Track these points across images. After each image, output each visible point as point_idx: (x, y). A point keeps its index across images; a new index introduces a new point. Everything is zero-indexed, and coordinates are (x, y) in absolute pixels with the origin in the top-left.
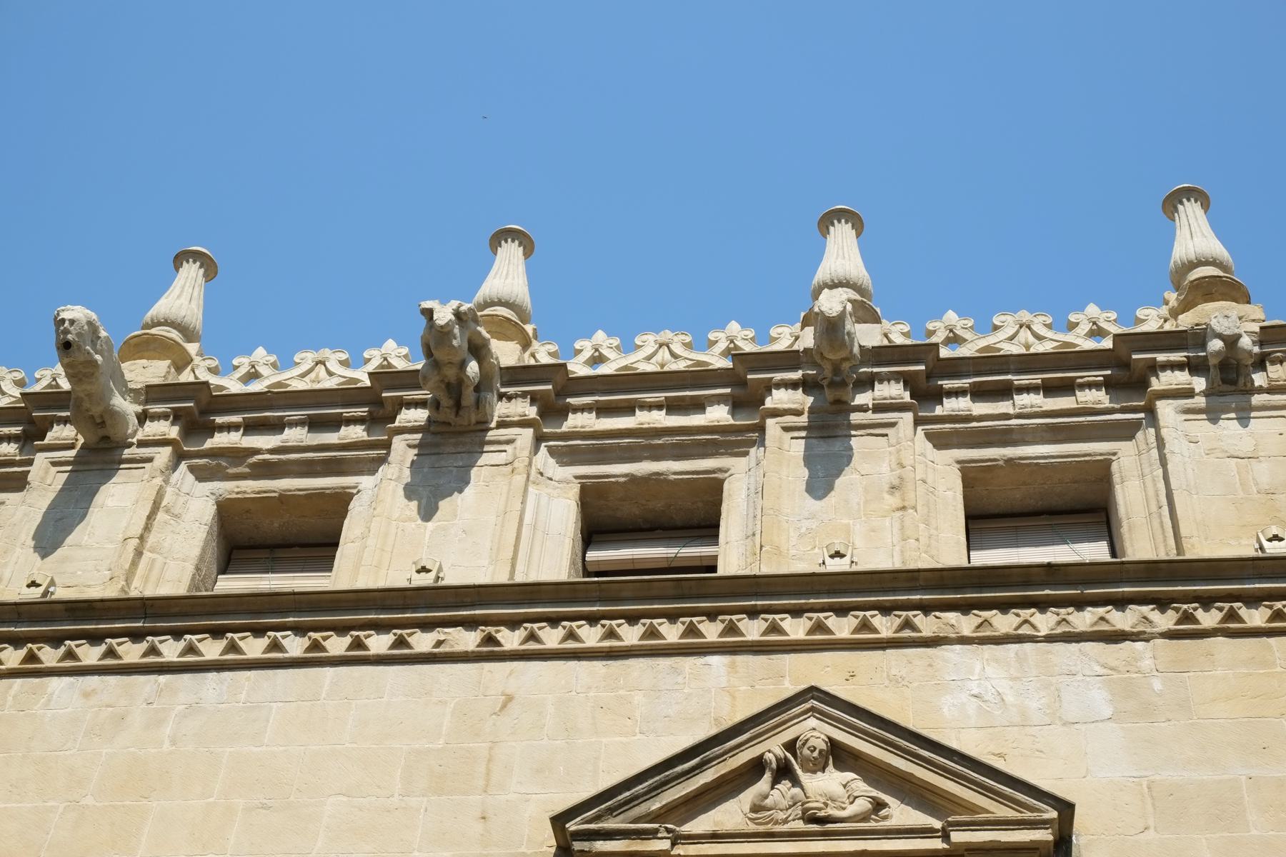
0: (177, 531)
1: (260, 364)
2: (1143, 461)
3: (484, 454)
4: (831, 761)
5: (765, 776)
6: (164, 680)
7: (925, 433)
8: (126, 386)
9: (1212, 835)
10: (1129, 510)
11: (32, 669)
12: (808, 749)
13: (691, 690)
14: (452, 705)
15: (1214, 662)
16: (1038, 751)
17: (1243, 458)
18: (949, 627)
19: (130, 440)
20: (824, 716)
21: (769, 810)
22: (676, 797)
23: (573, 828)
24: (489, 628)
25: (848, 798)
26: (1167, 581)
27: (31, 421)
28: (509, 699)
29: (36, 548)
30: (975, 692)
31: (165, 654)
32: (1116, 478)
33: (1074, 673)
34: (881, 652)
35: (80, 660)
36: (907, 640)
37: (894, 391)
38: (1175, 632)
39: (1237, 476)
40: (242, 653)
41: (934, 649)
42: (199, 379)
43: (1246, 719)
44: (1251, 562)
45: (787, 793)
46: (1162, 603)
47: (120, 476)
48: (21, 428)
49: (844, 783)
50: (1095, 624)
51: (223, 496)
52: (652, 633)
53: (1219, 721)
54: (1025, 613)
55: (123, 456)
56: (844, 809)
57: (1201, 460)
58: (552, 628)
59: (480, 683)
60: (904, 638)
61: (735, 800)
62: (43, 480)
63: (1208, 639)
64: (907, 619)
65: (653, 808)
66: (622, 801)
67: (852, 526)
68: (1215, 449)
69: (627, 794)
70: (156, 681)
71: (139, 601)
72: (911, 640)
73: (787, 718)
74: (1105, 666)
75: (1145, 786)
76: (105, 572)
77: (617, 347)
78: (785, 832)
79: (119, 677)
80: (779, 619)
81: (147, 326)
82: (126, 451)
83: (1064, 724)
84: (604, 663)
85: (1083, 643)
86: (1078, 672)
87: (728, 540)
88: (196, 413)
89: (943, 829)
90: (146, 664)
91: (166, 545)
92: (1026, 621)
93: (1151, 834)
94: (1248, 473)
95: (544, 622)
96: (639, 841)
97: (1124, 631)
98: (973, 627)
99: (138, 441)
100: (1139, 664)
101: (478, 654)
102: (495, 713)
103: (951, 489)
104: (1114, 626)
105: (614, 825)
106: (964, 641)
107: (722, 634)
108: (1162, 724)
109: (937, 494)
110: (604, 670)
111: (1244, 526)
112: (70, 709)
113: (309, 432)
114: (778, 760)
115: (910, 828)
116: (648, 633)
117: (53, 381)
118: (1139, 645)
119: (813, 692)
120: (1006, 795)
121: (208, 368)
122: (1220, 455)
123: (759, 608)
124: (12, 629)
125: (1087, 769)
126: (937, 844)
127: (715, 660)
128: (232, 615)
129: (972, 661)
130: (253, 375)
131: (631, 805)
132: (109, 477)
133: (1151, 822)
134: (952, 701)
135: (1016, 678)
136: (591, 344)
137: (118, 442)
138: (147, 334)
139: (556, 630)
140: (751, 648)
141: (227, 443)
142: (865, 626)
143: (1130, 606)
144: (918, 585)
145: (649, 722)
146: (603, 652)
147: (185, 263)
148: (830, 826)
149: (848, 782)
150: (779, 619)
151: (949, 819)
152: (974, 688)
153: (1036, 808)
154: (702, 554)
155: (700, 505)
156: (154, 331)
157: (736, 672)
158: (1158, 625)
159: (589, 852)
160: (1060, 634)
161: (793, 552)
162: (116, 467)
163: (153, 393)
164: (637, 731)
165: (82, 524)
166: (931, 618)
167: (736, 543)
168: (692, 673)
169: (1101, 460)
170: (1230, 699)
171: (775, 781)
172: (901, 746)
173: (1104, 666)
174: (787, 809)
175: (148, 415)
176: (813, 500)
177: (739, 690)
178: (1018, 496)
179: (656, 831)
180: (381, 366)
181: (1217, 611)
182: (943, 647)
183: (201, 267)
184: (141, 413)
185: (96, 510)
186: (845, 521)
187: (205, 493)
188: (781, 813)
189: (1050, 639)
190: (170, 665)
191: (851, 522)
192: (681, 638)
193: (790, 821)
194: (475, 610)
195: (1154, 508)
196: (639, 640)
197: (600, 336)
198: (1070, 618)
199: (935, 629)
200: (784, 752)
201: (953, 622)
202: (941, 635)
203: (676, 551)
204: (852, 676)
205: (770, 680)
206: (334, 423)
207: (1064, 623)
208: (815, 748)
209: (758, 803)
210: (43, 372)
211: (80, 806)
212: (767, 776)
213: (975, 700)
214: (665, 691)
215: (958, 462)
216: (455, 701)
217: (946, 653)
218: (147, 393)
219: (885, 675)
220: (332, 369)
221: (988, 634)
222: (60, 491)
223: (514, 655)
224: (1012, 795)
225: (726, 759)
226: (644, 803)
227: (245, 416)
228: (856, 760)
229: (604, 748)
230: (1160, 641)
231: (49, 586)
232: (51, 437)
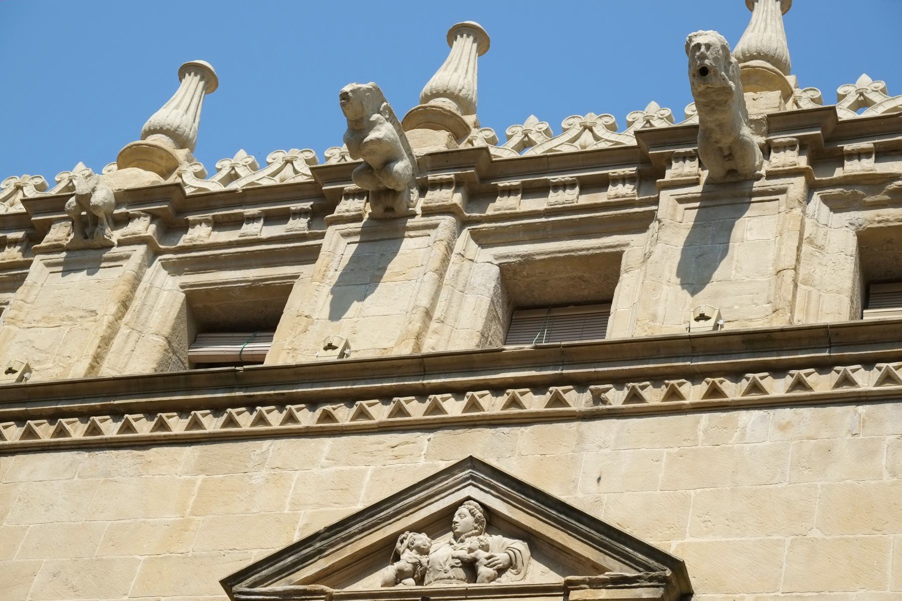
0: (824, 263)
3: (752, 205)
6: (864, 411)
7: (821, 197)
8: (747, 118)
11: (718, 402)
19: (758, 172)
27: (321, 195)
29: (684, 285)
31: (860, 384)
35: (766, 393)
37: (142, 227)
40: (522, 407)
42: (801, 107)
47: (754, 209)
48: (635, 168)
51: (863, 226)
55: (754, 189)
62: (673, 218)
70: (856, 412)
71: (824, 329)
76: (764, 305)
77: (883, 91)
79: (813, 408)
81: (427, 98)
82: (756, 184)
88: (477, 179)
90: (841, 394)
91: (817, 277)
99: (767, 172)
112: (768, 443)
113: (264, 224)
117: (232, 170)
121: (306, 160)
124: (688, 363)
128: (266, 387)
130: (233, 176)
132: (741, 212)
137: (746, 175)
138: (748, 66)
139: (783, 379)
141: (861, 170)
154: (254, 353)
156: (432, 103)
162: (748, 200)
163: (437, 160)
165: (726, 259)
175: (772, 146)
183: (201, 80)
184: (764, 145)
185: (737, 244)
187: (843, 224)
190: (868, 395)
192: (664, 400)
197: (864, 81)
206: (602, 184)
210: (635, 115)
211: (808, 539)
215: (182, 287)
218: (769, 123)
220: (297, 168)
222: (692, 228)
227: (876, 141)
231: (344, 349)
232: (670, 175)
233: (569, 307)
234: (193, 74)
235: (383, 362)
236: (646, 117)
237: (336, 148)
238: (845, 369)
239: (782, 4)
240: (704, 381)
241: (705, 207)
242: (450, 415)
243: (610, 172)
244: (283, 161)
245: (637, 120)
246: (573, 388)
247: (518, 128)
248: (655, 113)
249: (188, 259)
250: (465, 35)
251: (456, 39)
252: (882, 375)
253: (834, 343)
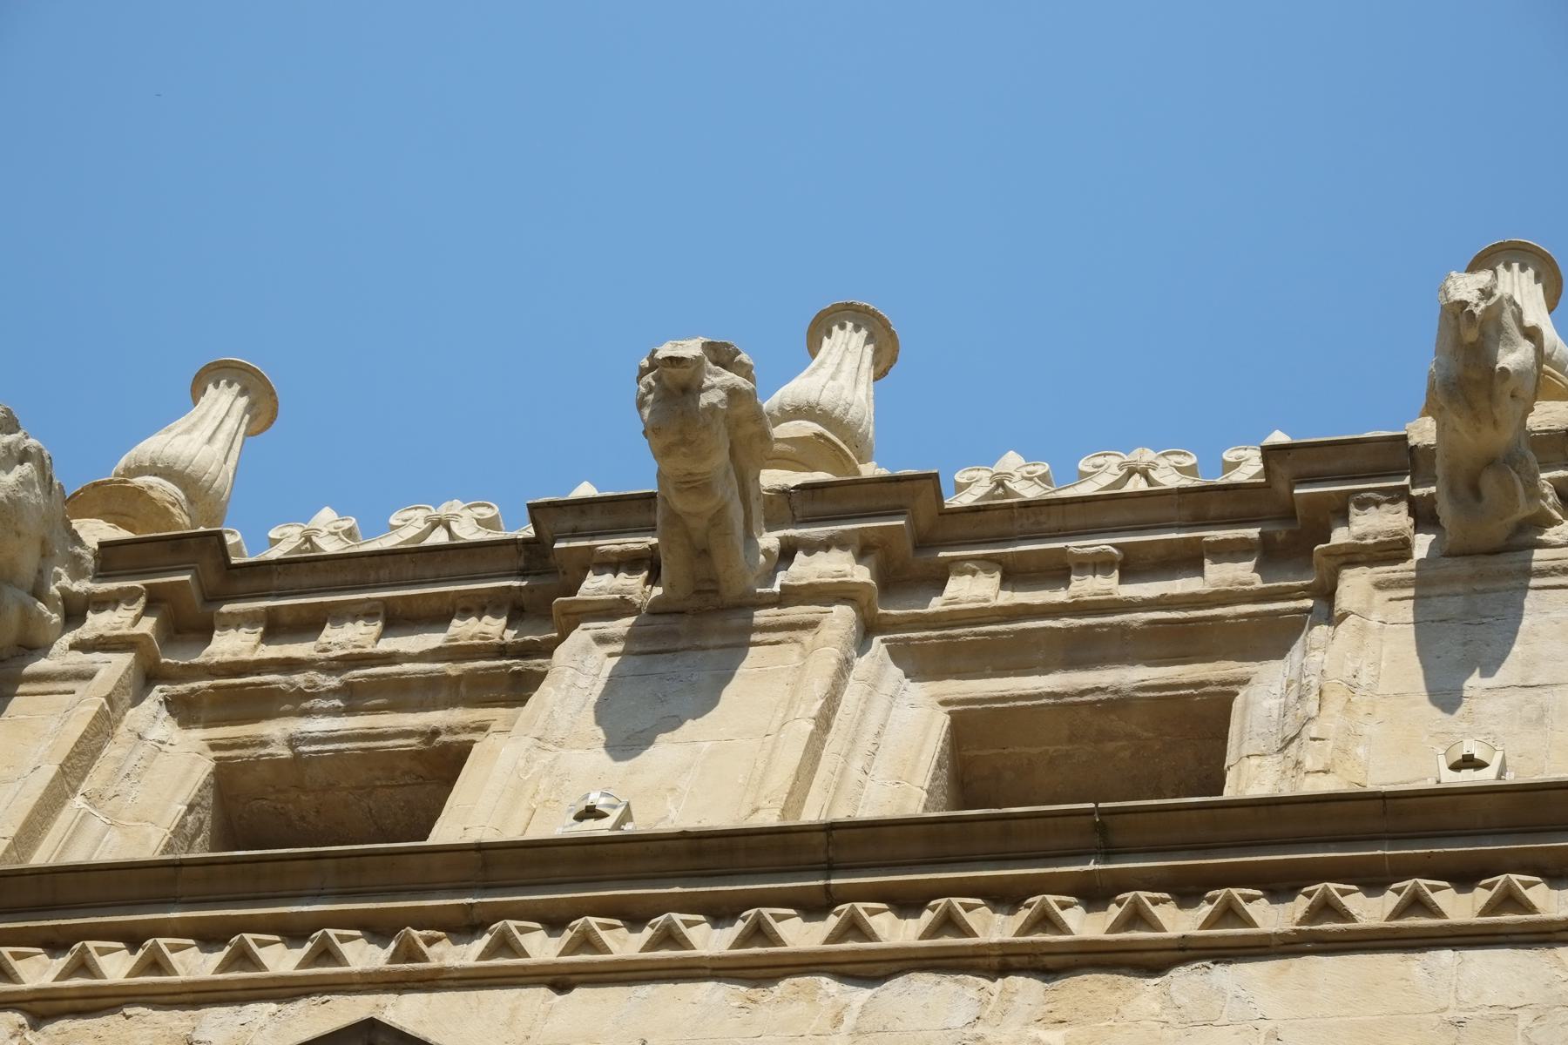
1: (321, 535)
27: (1288, 513)
35: (1162, 929)
64: (1325, 894)
95: (357, 929)
136: (990, 475)
139: (1470, 894)
140: (176, 998)
147: (210, 387)
156: (140, 481)
180: (298, 549)
183: (242, 393)
234: (850, 325)
235: (1350, 803)
236: (994, 476)
237: (979, 470)
239: (876, 352)
241: (1422, 597)
242: (790, 948)
243: (1074, 545)
244: (425, 523)
245: (977, 481)
246: (887, 907)
247: (981, 473)
248: (325, 526)
249: (917, 642)
250: (1516, 266)
251: (829, 334)
252: (746, 927)
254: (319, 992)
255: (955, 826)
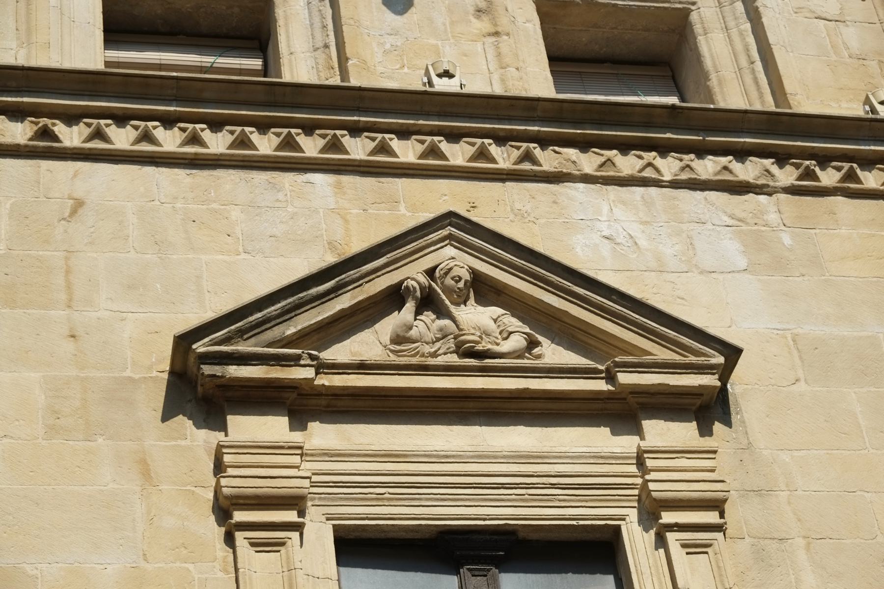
2: (725, 14)
4: (472, 294)
5: (407, 305)
9: (860, 390)
10: (717, 63)
11: (440, 166)
12: (452, 279)
13: (296, 210)
14: (8, 206)
15: (837, 221)
16: (679, 298)
17: (831, 21)
18: (570, 163)
20: (462, 245)
21: (414, 343)
22: (312, 322)
23: (202, 350)
24: (45, 119)
25: (501, 333)
26: (786, 135)
28: (79, 204)
30: (606, 233)
32: (698, 28)
33: (703, 221)
34: (500, 184)
36: (530, 174)
38: (798, 188)
39: (827, 37)
41: (556, 185)
43: (875, 279)
44: (868, 123)
45: (432, 325)
46: (782, 158)
49: (495, 317)
50: (719, 173)
52: (243, 142)
53: (850, 279)
54: (650, 156)
56: (498, 344)
57: (791, 18)
58: (119, 127)
59: (39, 183)
60: (525, 171)
61: (370, 330)
63: (828, 198)
64: (528, 151)
65: (289, 332)
66: (253, 323)
67: (441, 47)
68: (803, 8)
69: (259, 315)
72: (533, 174)
73: (424, 244)
74: (733, 217)
75: (789, 339)
78: (440, 365)
80: (389, 138)
83: (701, 273)
84: (188, 171)
85: (707, 192)
86: (707, 221)
87: (293, 50)
89: (608, 370)
92: (650, 164)
93: (802, 386)
94: (838, 36)
96: (278, 367)
97: (748, 182)
98: (595, 165)
100: (765, 217)
101: (33, 149)
102: (64, 219)
103: (531, 21)
104: (737, 177)
105: (250, 349)
106: (587, 179)
107: (323, 150)
108: (796, 279)
109: (516, 24)
110: (188, 180)
111: (842, 89)
114: (422, 288)
115: (574, 368)
116: (238, 142)
118: (762, 198)
119: (450, 218)
120: (671, 338)
122: (808, 15)
123: (361, 125)
125: (732, 319)
126: (601, 385)
127: (319, 178)
129: (597, 201)
131: (263, 328)
133: (801, 374)
134: (584, 241)
135: (646, 222)
140: (358, 169)
142: (483, 154)
143: (751, 158)
144: (536, 115)
145: (252, 241)
146: (185, 159)
148: (489, 362)
149: (499, 317)
150: (389, 138)
151: (617, 359)
152: (604, 229)
153: (702, 353)
155: (236, 10)
157: (345, 193)
158: (779, 179)
159: (222, 377)
160: (686, 180)
161: (380, 69)
164: (241, 249)
166: (549, 152)
167: (302, 55)
168: (293, 191)
169: (679, 9)
170: (857, 259)
171: (418, 312)
172: (553, 282)
173: (732, 217)
174: (433, 343)
176: (393, 15)
177: (351, 213)
178: (584, 39)
179: (299, 357)
181: (834, 171)
182: (566, 184)
186: (432, 41)
188: (427, 346)
189: (675, 184)
191: (439, 43)
192: (275, 150)
193: (440, 355)
194: (22, 97)
195: (744, 62)
196: (227, 149)
198: (693, 164)
199: (555, 164)
200: (428, 281)
201: (574, 158)
202: (564, 171)
203: (212, 61)
204: (473, 207)
205: (383, 205)
207: (688, 169)
208: (460, 279)
209: (402, 334)
212: (410, 306)
213: (607, 242)
214: (266, 209)
216: (10, 202)
217: (569, 191)
219: (509, 209)
221: (611, 173)
223: (76, 154)
224: (676, 338)
225: (361, 285)
226: (277, 327)
228: (499, 295)
229: (204, 265)
230: (783, 196)
233: (178, 37)
235: (115, 77)
238: (383, 136)
240: (175, 126)
253: (746, 129)
254: (557, 181)
255: (787, 118)
